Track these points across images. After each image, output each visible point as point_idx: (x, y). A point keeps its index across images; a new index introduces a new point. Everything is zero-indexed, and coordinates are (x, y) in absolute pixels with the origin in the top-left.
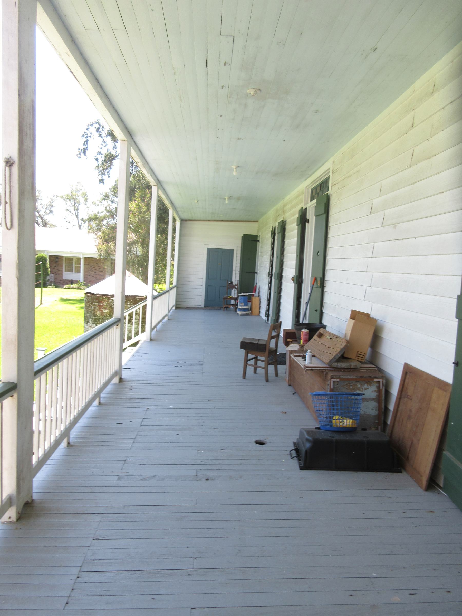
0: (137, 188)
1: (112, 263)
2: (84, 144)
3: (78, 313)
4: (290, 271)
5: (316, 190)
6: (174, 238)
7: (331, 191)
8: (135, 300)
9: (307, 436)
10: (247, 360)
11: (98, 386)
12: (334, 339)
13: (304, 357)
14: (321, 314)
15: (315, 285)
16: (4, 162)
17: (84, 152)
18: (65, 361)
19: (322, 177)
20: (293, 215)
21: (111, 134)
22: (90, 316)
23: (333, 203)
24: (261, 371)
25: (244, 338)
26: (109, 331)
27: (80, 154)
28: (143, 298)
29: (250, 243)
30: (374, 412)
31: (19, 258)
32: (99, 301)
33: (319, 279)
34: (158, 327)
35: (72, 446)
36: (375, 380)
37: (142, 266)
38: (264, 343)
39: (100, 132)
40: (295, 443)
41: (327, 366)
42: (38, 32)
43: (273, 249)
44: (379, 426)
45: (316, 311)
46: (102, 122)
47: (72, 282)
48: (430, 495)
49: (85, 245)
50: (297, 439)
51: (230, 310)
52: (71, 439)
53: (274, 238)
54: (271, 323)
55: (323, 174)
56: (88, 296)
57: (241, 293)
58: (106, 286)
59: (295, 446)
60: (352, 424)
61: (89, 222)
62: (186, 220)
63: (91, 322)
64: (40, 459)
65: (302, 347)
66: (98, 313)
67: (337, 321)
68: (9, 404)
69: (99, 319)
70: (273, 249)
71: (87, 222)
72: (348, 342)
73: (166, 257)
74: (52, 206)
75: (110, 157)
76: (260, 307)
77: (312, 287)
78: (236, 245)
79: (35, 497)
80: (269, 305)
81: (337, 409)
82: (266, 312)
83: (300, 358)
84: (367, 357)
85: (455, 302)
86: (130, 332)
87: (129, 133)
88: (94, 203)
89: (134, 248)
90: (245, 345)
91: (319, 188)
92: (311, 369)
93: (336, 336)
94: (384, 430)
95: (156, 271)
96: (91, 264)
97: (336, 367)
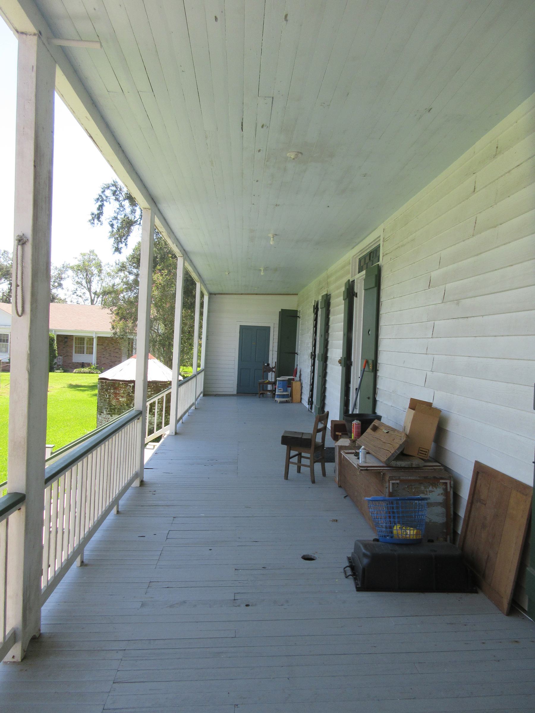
0: (161, 258)
1: (129, 344)
2: (99, 209)
3: (90, 402)
4: (336, 352)
5: (365, 259)
6: (201, 314)
7: (382, 261)
8: (157, 386)
9: (364, 551)
10: (289, 458)
11: (116, 491)
12: (391, 432)
13: (357, 455)
14: (375, 402)
15: (366, 369)
16: (16, 240)
17: (98, 218)
18: (80, 464)
19: (372, 246)
20: (338, 288)
21: (130, 198)
22: (104, 405)
25: (286, 432)
26: (129, 427)
27: (94, 220)
28: (166, 385)
29: (289, 319)
31: (31, 348)
32: (115, 388)
33: (370, 362)
34: (184, 418)
35: (86, 565)
36: (441, 481)
37: (163, 346)
38: (310, 437)
39: (118, 195)
40: (349, 559)
41: (384, 465)
42: (57, 99)
43: (315, 326)
44: (448, 537)
45: (369, 398)
46: (120, 183)
47: (83, 365)
48: (513, 622)
49: (99, 322)
50: (352, 554)
51: (267, 397)
52: (85, 558)
53: (316, 314)
54: (315, 411)
55: (372, 242)
56: (102, 382)
57: (279, 377)
58: (125, 371)
59: (350, 562)
60: (417, 534)
61: (103, 296)
62: (215, 294)
63: (105, 412)
64: (49, 583)
65: (354, 441)
66: (114, 402)
67: (393, 410)
68: (16, 518)
69: (114, 409)
70: (315, 326)
71: (101, 296)
72: (407, 436)
73: (193, 336)
74: (62, 279)
75: (128, 223)
76: (302, 392)
77: (363, 372)
78: (273, 323)
79: (43, 630)
80: (312, 390)
81: (398, 517)
82: (309, 399)
83: (352, 456)
84: (431, 453)
86: (151, 423)
87: (152, 200)
88: (109, 274)
89: (155, 326)
90: (290, 441)
91: (368, 258)
92: (366, 469)
93: (394, 430)
94: (454, 541)
95: (182, 352)
96: (105, 345)
97: (394, 465)
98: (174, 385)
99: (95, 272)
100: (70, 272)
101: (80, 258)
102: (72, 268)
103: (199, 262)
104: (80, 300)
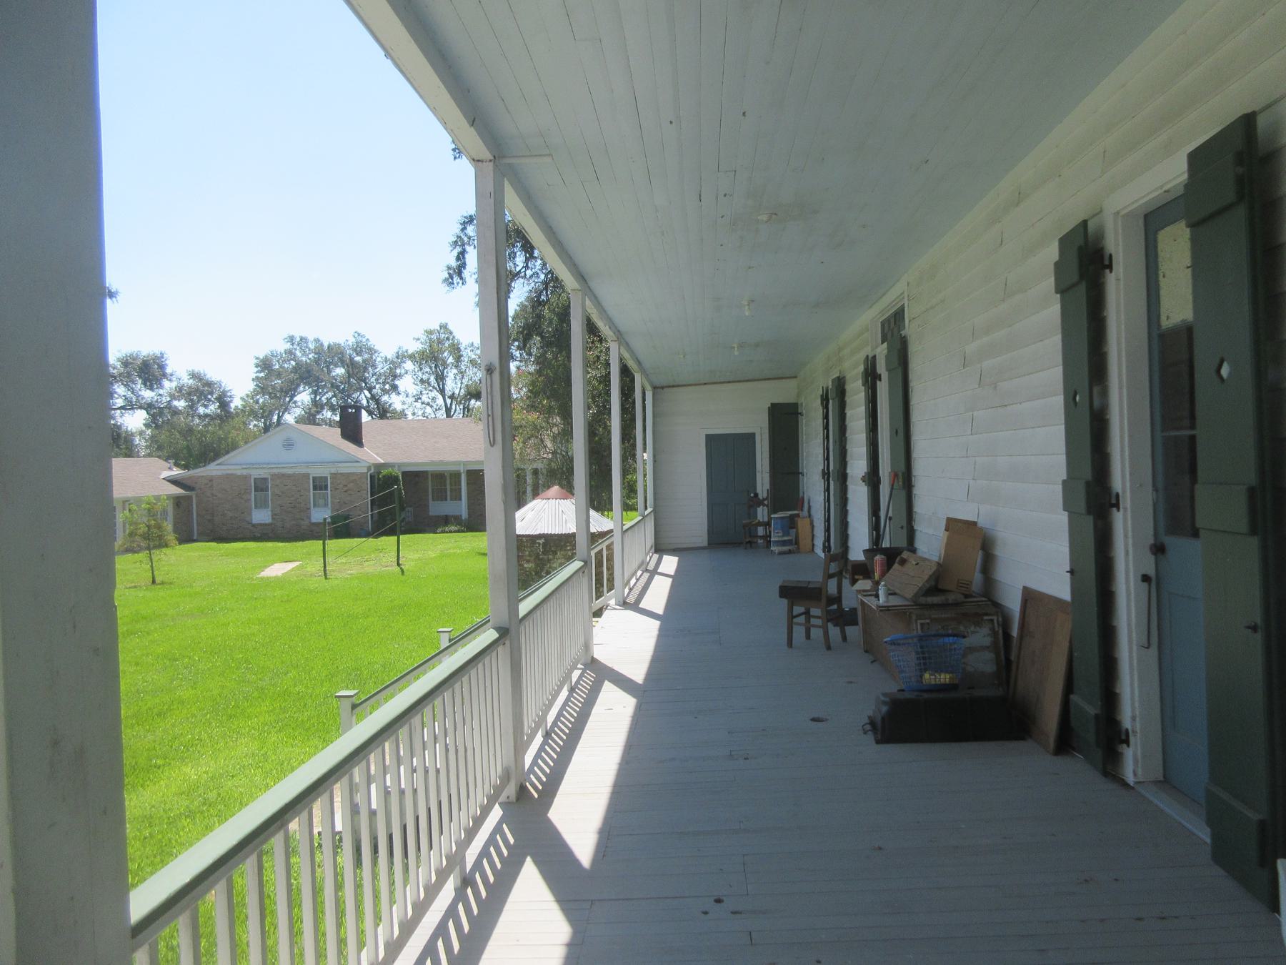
2: (458, 259)
4: (858, 466)
7: (910, 329)
10: (791, 617)
13: (877, 596)
17: (460, 274)
23: (913, 348)
24: (817, 633)
30: (990, 668)
48: (1063, 763)
62: (663, 388)
70: (826, 427)
78: (757, 425)
80: (828, 530)
85: (1060, 487)
90: (791, 593)
92: (886, 609)
98: (617, 534)
99: (451, 360)
100: (409, 365)
101: (423, 338)
102: (412, 357)
103: (639, 345)
104: (428, 410)
